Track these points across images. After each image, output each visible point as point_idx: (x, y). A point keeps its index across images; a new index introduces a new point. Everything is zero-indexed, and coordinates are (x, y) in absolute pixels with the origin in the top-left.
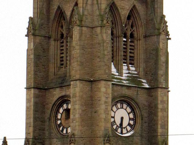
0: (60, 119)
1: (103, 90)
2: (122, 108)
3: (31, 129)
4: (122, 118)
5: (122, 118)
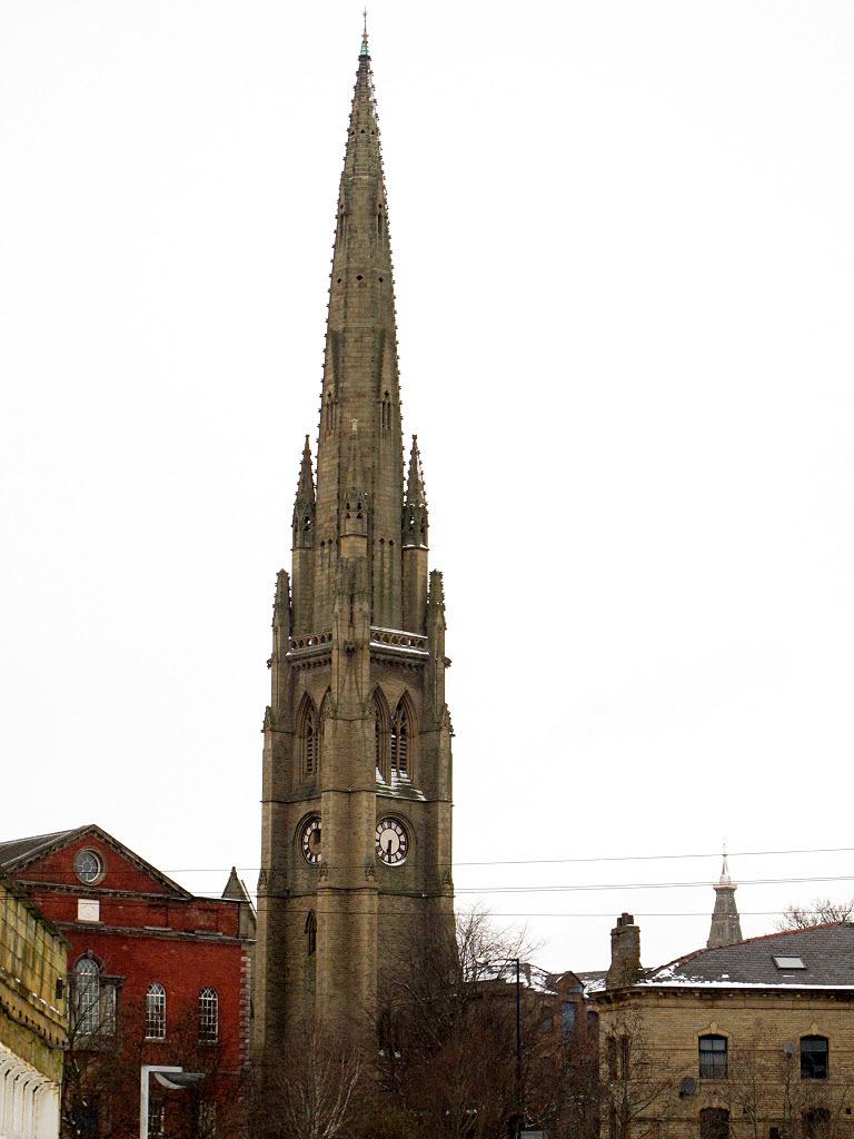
0: (308, 843)
1: (365, 804)
2: (390, 828)
3: (269, 856)
4: (390, 842)
5: (390, 842)
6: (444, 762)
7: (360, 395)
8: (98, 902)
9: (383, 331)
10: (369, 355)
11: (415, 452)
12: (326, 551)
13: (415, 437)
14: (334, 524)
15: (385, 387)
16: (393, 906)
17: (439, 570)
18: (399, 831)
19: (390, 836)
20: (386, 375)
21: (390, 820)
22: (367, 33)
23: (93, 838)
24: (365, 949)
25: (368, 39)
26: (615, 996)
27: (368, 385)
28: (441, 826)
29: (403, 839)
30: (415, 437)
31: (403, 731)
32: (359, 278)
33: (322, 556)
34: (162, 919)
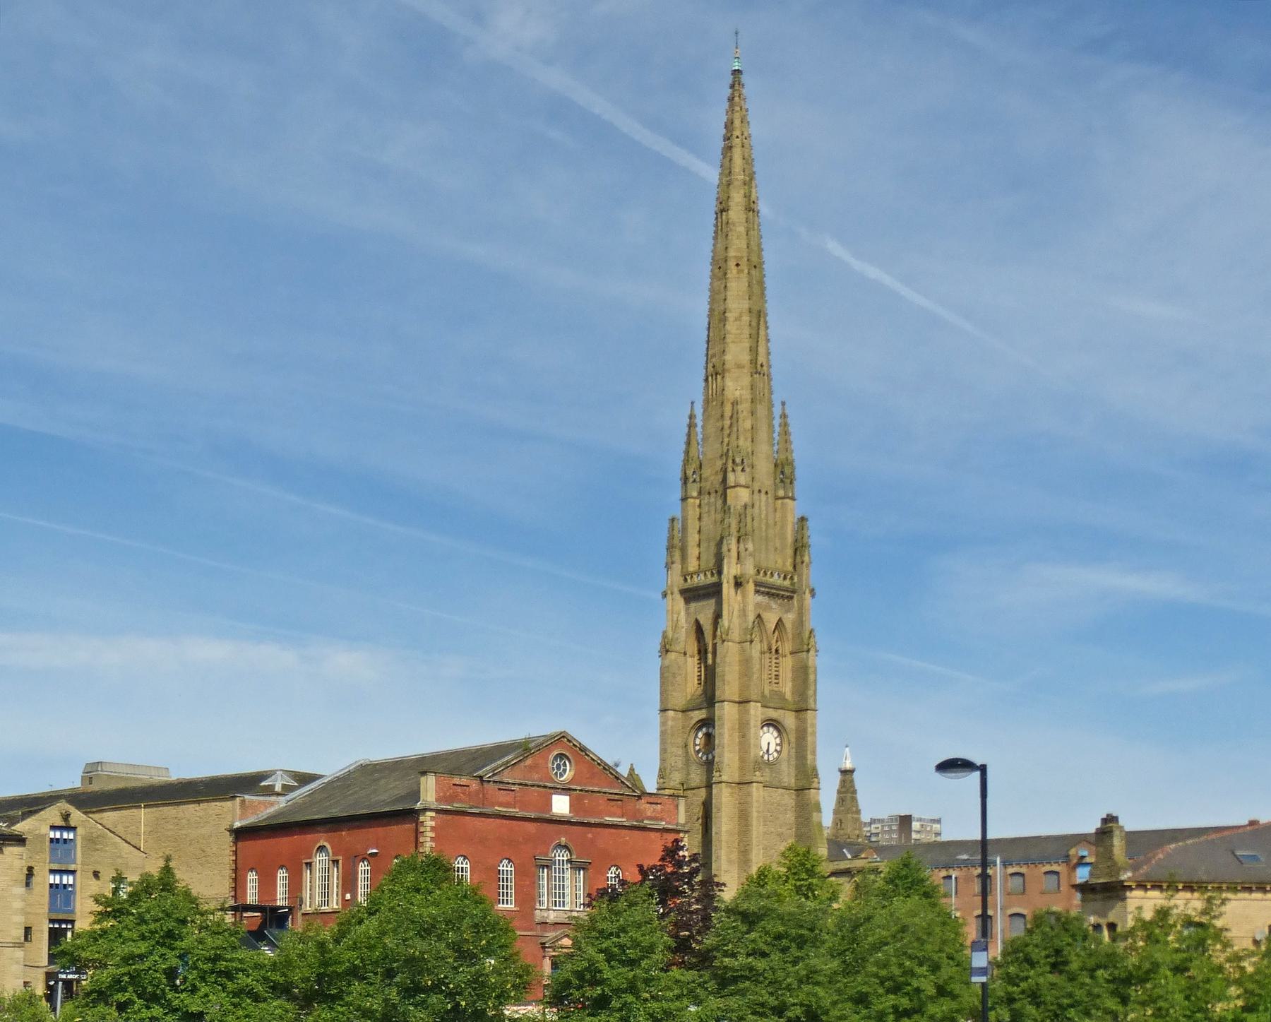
6: (812, 677)
7: (740, 366)
8: (567, 798)
9: (760, 312)
10: (747, 331)
11: (784, 416)
12: (712, 500)
13: (783, 404)
14: (720, 477)
15: (761, 359)
16: (1089, 994)
17: (806, 515)
18: (776, 734)
19: (769, 738)
20: (762, 350)
21: (768, 725)
22: (787, 412)
23: (564, 746)
24: (724, 837)
25: (789, 420)
26: (1064, 924)
27: (745, 358)
28: (810, 730)
29: (778, 741)
30: (783, 404)
31: (777, 651)
32: (737, 265)
33: (709, 504)
34: (619, 812)
